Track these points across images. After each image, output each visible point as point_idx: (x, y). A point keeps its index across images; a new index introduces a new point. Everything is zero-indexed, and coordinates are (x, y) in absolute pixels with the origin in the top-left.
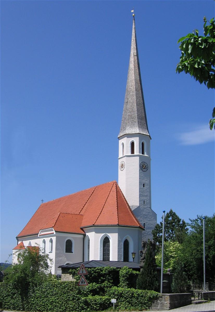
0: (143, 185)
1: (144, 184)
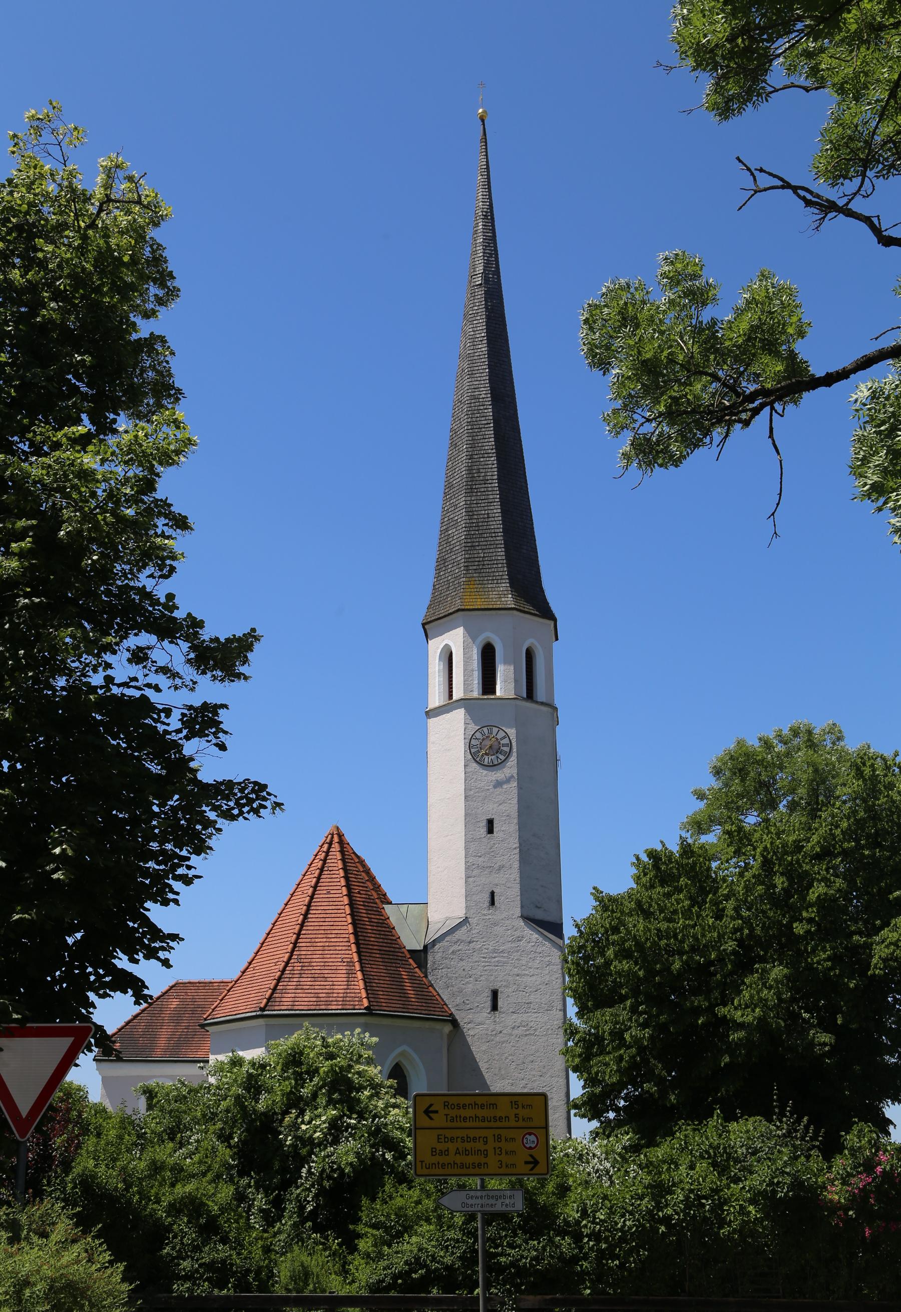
0: (484, 823)
1: (490, 822)
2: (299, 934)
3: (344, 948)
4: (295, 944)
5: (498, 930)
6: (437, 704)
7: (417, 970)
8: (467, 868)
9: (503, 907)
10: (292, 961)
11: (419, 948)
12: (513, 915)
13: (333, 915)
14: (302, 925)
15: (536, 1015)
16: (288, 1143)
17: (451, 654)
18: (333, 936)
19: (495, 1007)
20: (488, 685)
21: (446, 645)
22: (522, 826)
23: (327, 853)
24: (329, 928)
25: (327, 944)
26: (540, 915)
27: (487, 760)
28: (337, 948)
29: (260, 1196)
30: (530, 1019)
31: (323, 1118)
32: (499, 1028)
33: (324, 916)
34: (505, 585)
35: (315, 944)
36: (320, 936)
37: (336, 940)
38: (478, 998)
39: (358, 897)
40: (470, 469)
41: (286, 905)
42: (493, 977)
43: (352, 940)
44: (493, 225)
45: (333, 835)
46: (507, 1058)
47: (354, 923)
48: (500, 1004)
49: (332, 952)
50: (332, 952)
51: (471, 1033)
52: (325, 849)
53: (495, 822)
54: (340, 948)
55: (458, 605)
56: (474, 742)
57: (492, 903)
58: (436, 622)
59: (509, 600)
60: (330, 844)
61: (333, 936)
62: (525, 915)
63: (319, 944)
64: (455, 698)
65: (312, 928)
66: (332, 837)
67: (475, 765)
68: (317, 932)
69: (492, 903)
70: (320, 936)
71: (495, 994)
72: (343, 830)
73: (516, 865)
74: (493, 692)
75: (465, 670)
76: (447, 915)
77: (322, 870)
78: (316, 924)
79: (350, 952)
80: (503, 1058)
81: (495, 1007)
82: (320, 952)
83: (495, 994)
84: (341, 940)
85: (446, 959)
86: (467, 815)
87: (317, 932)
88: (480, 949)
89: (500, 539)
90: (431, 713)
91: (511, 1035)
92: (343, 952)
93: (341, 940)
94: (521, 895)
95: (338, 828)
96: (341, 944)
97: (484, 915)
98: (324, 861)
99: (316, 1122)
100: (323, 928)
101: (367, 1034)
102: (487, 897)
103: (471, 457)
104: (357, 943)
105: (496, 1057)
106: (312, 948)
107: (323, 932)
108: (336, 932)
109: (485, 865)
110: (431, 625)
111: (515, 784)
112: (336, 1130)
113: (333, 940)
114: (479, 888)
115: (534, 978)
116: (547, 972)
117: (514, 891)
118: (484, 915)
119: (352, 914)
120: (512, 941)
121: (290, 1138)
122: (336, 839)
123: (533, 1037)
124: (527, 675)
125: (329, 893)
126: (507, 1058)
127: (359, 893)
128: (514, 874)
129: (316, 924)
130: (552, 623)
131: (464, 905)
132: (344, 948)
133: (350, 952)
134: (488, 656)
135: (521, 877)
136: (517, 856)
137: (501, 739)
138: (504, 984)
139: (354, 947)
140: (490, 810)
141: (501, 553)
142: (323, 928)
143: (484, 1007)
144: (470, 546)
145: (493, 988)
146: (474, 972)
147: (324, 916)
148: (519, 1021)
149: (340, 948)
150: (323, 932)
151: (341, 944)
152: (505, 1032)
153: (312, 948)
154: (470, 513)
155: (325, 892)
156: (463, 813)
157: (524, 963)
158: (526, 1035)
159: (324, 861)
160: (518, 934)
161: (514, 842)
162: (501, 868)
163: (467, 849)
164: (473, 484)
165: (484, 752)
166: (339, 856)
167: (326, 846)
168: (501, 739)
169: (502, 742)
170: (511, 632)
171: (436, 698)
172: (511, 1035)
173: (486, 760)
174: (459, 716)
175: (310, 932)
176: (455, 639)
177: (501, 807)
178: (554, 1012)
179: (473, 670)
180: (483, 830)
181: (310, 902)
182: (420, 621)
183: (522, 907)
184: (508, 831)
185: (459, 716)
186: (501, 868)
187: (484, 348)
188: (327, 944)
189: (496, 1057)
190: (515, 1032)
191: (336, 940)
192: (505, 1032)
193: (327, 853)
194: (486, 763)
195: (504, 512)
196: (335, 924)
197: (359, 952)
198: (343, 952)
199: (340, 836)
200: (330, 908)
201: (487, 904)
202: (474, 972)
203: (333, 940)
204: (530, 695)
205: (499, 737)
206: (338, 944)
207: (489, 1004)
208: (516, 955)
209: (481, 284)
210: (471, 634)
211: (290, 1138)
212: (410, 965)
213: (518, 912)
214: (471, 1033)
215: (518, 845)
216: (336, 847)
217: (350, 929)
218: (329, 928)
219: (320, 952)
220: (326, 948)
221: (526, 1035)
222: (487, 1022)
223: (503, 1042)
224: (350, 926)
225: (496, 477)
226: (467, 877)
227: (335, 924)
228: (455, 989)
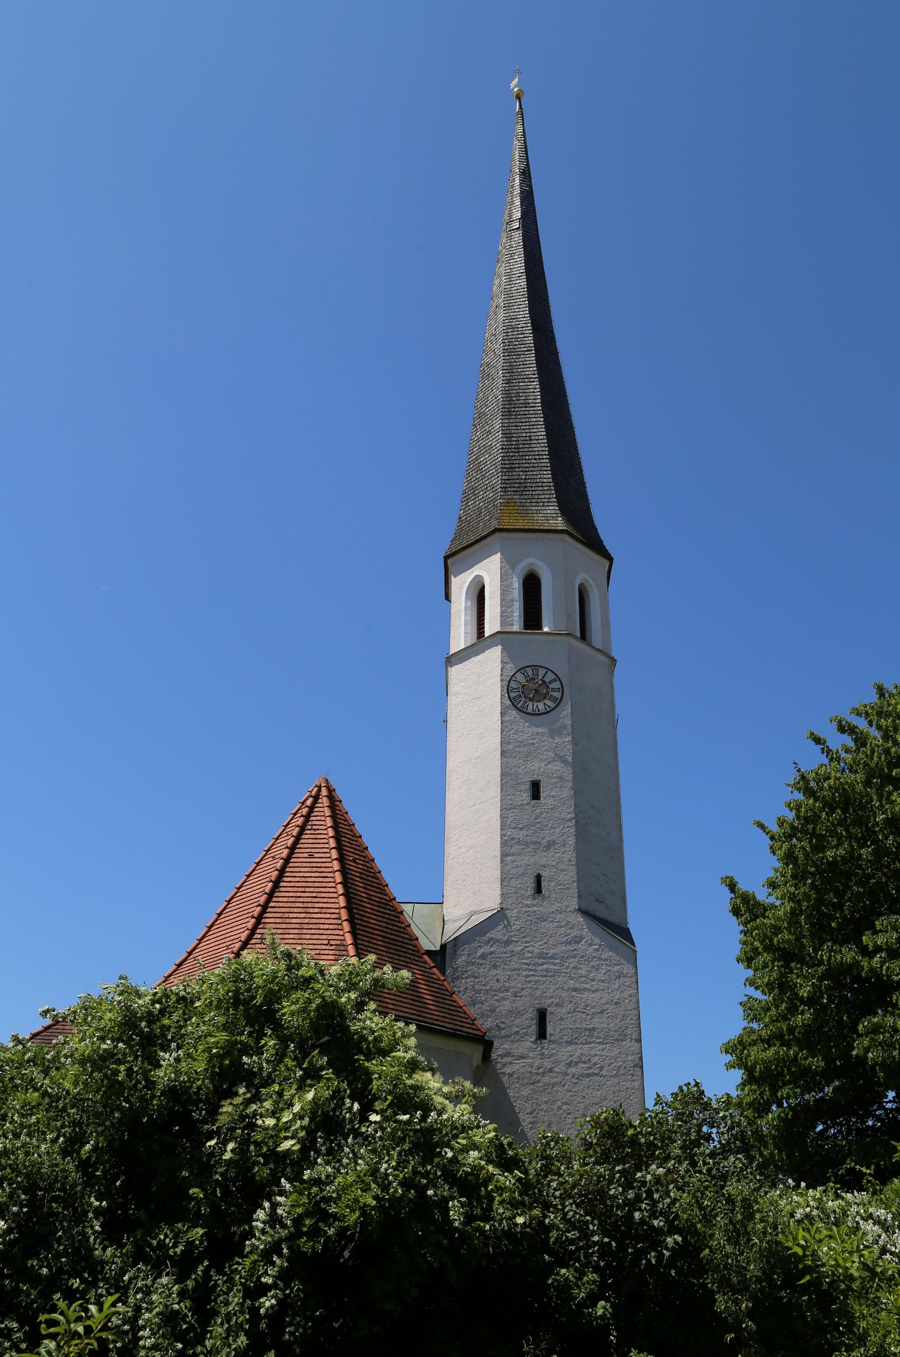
0: (528, 786)
2: (265, 907)
3: (331, 927)
4: (259, 919)
5: (546, 926)
6: (462, 647)
7: (435, 970)
8: (503, 844)
9: (553, 895)
10: (253, 941)
11: (433, 949)
12: (567, 906)
13: (317, 885)
14: (271, 895)
15: (601, 1047)
16: (227, 1156)
17: (483, 587)
18: (316, 910)
19: (542, 1034)
20: (532, 617)
21: (476, 576)
22: (578, 793)
23: (312, 808)
24: (310, 900)
25: (307, 921)
26: (601, 912)
27: (530, 707)
28: (322, 926)
29: (164, 1280)
30: (593, 1052)
31: (297, 1108)
32: (547, 1064)
33: (304, 884)
34: (553, 509)
35: (288, 921)
36: (296, 910)
37: (319, 916)
38: (518, 1021)
39: (352, 866)
40: (507, 395)
41: (248, 876)
42: (539, 993)
43: (344, 914)
44: (530, 181)
45: (320, 787)
46: (559, 1108)
47: (347, 895)
48: (549, 1029)
49: (313, 931)
50: (313, 931)
51: (508, 1070)
52: (309, 802)
53: (542, 785)
54: (326, 927)
55: (494, 524)
56: (513, 685)
57: (539, 890)
58: (463, 553)
59: (559, 523)
60: (316, 798)
61: (316, 910)
62: (584, 908)
63: (294, 921)
64: (487, 633)
65: (285, 899)
66: (319, 790)
67: (514, 712)
68: (293, 905)
69: (539, 890)
70: (296, 910)
71: (542, 1015)
72: (334, 784)
73: (572, 841)
74: (539, 626)
75: (502, 601)
76: (474, 908)
77: (303, 828)
78: (291, 894)
79: (341, 933)
80: (555, 1107)
81: (542, 1034)
82: (296, 931)
83: (542, 1015)
84: (328, 916)
85: (473, 964)
86: (503, 775)
87: (293, 905)
88: (521, 953)
89: (546, 461)
90: (451, 660)
91: (565, 1074)
92: (330, 932)
93: (328, 916)
94: (578, 881)
95: (327, 781)
96: (327, 921)
97: (527, 906)
98: (307, 818)
99: (285, 1113)
100: (302, 900)
101: (388, 968)
102: (530, 882)
103: (508, 382)
104: (351, 920)
105: (544, 1107)
106: (284, 926)
107: (301, 905)
108: (321, 905)
109: (529, 839)
110: (458, 554)
111: (569, 738)
112: (326, 1125)
113: (315, 916)
114: (521, 870)
115: (598, 994)
116: (616, 986)
117: (570, 875)
118: (527, 906)
119: (344, 883)
120: (567, 943)
121: (231, 1146)
122: (324, 792)
123: (597, 1078)
124: (580, 614)
125: (311, 856)
126: (559, 1108)
127: (354, 861)
128: (570, 854)
129: (291, 894)
130: (607, 563)
131: (499, 892)
132: (331, 927)
133: (341, 933)
134: (531, 586)
135: (577, 857)
136: (573, 830)
137: (550, 682)
138: (556, 1001)
139: (346, 926)
140: (537, 768)
141: (547, 476)
142: (302, 900)
143: (526, 1034)
144: (508, 467)
145: (538, 1006)
146: (513, 984)
147: (304, 884)
148: (578, 1054)
149: (326, 927)
150: (301, 905)
151: (327, 921)
152: (556, 1069)
153: (284, 926)
154: (508, 435)
155: (306, 855)
156: (498, 772)
157: (583, 972)
158: (588, 1075)
159: (307, 818)
160: (575, 933)
161: (568, 812)
162: (550, 845)
163: (503, 818)
164: (511, 407)
165: (528, 694)
166: (328, 812)
167: (311, 800)
168: (550, 682)
169: (551, 686)
170: (560, 566)
171: (460, 636)
172: (565, 1074)
173: (530, 707)
174: (493, 656)
175: (282, 905)
176: (490, 570)
177: (549, 766)
178: (627, 1043)
179: (513, 601)
180: (526, 796)
181: (284, 866)
182: (443, 554)
183: (580, 897)
184: (559, 796)
185: (493, 656)
186: (550, 845)
187: (523, 282)
188: (307, 921)
189: (544, 1107)
190: (572, 1070)
191: (319, 916)
192: (556, 1069)
193: (312, 808)
194: (530, 711)
195: (549, 436)
196: (319, 895)
197: (353, 932)
198: (330, 932)
199: (331, 791)
200: (313, 875)
201: (530, 891)
202: (513, 984)
203: (315, 916)
204: (584, 636)
205: (547, 679)
206: (323, 921)
207: (533, 1029)
208: (573, 962)
209: (518, 228)
210: (509, 563)
211: (231, 1146)
212: (425, 963)
213: (574, 904)
214: (508, 1070)
215: (573, 815)
216: (324, 801)
217: (342, 901)
218: (310, 900)
219: (296, 931)
220: (306, 926)
221: (588, 1075)
222: (531, 1054)
223: (554, 1085)
224: (341, 898)
225: (539, 401)
226: (504, 855)
227: (319, 895)
228: (485, 1007)
